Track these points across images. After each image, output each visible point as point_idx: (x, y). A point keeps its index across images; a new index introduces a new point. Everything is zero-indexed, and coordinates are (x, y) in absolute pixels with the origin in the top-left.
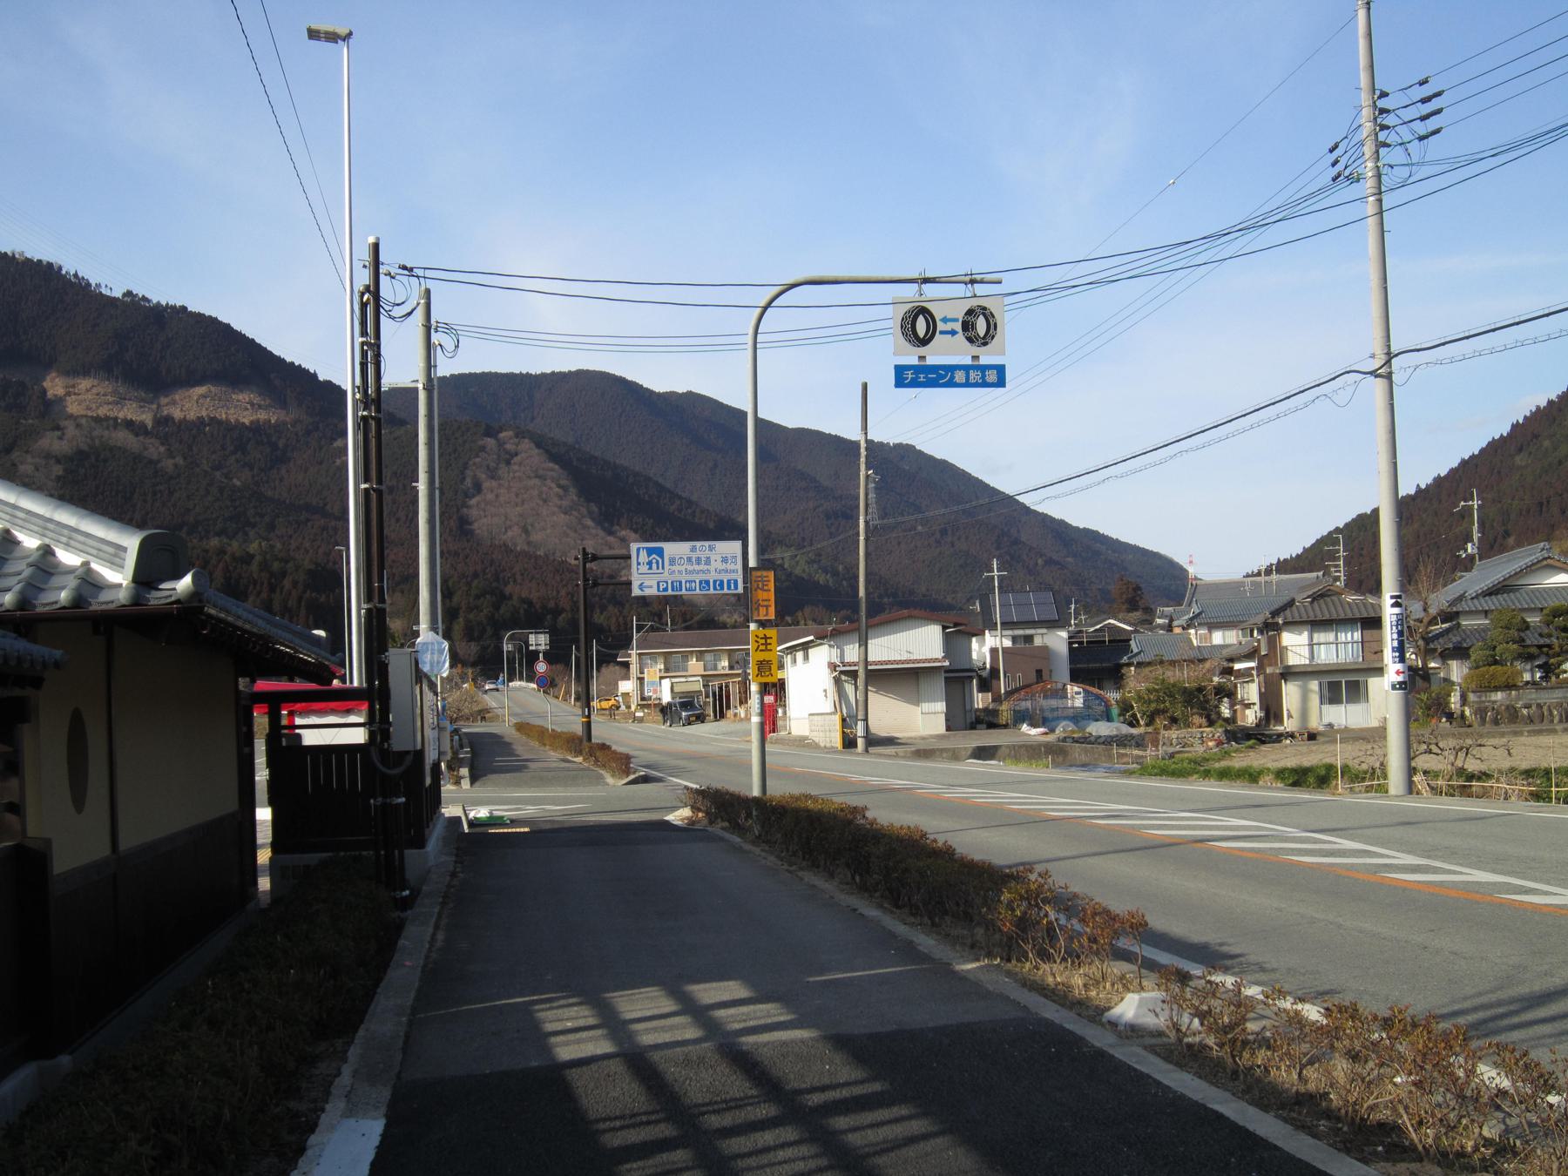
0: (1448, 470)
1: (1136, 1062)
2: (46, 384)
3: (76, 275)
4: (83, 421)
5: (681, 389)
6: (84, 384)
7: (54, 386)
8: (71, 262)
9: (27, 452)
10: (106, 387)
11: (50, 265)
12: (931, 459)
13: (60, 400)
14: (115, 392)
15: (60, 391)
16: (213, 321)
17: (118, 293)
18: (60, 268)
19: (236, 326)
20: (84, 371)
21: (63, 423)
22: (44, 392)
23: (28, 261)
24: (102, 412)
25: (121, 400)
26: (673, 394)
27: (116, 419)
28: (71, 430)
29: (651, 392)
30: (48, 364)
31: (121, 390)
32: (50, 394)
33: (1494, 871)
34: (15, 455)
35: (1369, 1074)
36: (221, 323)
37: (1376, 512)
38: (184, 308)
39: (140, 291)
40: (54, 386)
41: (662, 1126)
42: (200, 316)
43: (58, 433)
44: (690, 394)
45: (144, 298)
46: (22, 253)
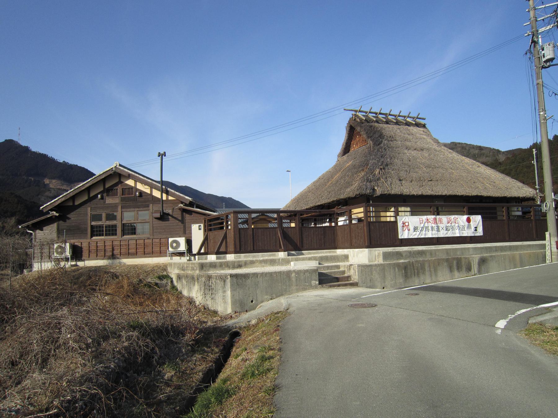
0: (26, 145)
1: (335, 275)
2: (45, 181)
3: (51, 157)
4: (56, 189)
5: (184, 185)
6: (54, 181)
7: (47, 181)
8: (50, 154)
9: (42, 196)
10: (59, 182)
11: (45, 155)
12: (235, 200)
13: (48, 184)
14: (61, 183)
15: (48, 182)
16: (84, 168)
17: (61, 161)
18: (48, 155)
19: (89, 169)
20: (54, 178)
21: (51, 190)
22: (44, 182)
23: (40, 154)
24: (58, 187)
25: (63, 185)
26: (182, 186)
27: (62, 189)
28: (53, 191)
29: (178, 186)
30: (45, 177)
31: (63, 183)
32: (46, 183)
33: (142, 266)
34: (40, 196)
35: (239, 292)
36: (85, 169)
37: (95, 175)
38: (77, 165)
39: (67, 161)
40: (47, 181)
41: (257, 292)
42: (81, 167)
43: (50, 192)
44: (186, 186)
45: (68, 163)
46: (38, 152)
